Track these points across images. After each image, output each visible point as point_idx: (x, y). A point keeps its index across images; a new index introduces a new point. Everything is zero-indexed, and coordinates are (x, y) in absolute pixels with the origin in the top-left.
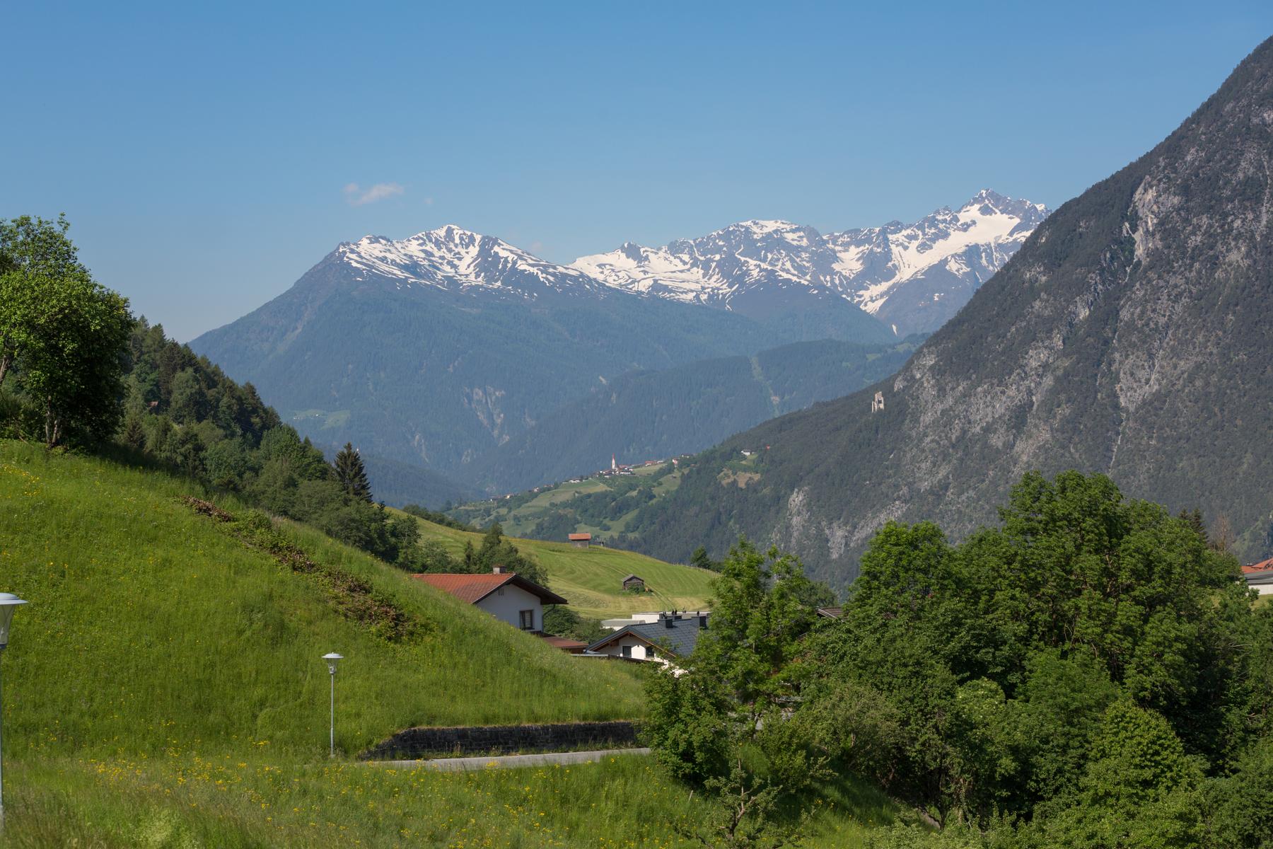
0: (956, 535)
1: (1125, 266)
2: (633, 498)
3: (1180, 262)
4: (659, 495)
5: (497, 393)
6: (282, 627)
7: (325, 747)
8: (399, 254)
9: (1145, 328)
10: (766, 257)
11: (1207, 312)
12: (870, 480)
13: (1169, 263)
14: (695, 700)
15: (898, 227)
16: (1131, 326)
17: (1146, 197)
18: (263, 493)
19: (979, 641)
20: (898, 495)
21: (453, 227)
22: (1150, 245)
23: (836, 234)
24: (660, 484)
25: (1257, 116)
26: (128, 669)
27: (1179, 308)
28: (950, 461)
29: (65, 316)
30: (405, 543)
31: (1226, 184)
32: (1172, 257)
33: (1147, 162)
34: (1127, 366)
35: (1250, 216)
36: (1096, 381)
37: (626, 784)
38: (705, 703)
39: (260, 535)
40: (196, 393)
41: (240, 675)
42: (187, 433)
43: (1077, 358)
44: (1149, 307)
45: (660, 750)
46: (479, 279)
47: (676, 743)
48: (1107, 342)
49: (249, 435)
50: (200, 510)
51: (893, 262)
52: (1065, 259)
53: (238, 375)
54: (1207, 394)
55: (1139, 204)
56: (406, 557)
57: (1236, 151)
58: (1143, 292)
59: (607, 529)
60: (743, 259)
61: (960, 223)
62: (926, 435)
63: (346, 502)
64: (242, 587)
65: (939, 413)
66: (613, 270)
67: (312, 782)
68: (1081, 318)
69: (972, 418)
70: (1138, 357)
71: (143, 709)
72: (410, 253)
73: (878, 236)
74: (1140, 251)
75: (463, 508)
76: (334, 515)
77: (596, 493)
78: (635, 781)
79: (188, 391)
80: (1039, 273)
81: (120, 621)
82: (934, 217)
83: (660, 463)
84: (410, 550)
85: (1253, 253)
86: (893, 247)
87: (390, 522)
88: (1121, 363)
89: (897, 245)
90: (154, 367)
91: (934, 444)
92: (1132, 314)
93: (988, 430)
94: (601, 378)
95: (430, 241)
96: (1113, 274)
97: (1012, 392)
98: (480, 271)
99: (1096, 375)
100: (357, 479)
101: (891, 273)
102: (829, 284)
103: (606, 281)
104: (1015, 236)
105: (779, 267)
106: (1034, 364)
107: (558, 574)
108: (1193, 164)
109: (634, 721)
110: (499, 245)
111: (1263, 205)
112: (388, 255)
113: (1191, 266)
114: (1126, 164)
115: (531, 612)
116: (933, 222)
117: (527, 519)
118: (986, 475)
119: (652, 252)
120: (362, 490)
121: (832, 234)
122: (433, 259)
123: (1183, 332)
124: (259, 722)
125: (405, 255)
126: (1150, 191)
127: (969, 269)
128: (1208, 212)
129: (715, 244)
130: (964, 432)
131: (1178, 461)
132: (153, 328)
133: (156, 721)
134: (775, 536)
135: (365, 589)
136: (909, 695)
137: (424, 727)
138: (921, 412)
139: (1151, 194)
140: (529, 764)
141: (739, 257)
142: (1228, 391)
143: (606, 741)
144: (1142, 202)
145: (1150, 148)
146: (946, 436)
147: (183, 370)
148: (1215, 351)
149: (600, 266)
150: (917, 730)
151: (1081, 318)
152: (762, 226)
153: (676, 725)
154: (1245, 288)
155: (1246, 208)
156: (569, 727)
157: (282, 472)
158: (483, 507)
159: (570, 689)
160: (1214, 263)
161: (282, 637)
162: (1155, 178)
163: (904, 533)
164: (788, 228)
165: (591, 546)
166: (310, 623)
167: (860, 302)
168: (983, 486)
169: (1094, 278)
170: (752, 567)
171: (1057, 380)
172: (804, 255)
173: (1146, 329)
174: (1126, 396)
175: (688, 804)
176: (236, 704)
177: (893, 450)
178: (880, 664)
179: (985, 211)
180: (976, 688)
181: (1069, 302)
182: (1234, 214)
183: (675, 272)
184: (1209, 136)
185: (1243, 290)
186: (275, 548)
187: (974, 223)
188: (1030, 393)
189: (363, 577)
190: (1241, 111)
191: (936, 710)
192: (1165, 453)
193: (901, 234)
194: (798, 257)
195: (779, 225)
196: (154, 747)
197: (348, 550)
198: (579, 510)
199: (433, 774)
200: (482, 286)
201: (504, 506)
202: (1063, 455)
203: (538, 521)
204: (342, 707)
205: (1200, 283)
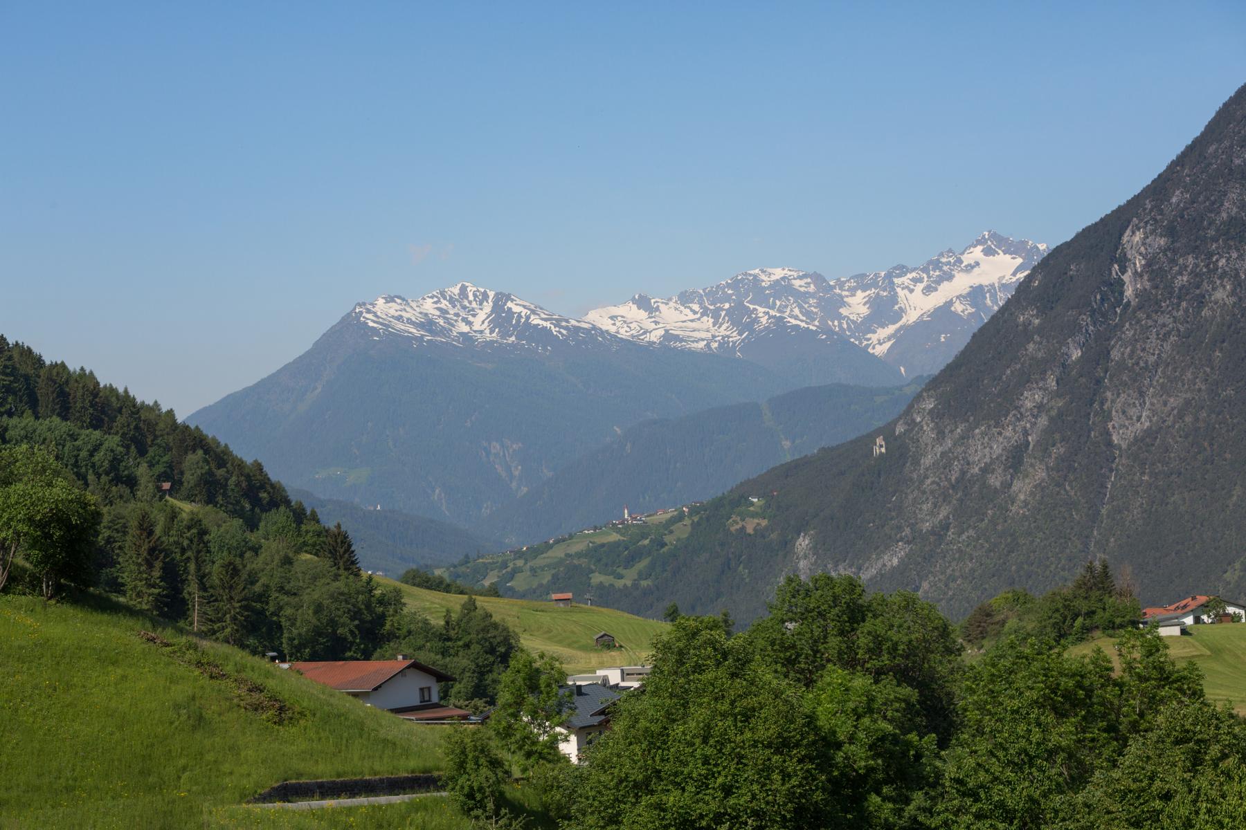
0: (957, 574)
1: (1115, 308)
2: (645, 546)
3: (1168, 302)
5: (514, 446)
6: (200, 718)
8: (414, 312)
9: (1135, 367)
10: (774, 304)
12: (874, 522)
13: (1157, 303)
15: (902, 270)
16: (1121, 365)
17: (1134, 239)
18: (263, 571)
20: (901, 537)
21: (467, 284)
22: (1138, 286)
23: (842, 279)
24: (671, 532)
25: (1238, 157)
27: (1167, 347)
28: (950, 502)
29: (54, 514)
30: (391, 611)
31: (1210, 224)
34: (1118, 405)
35: (1235, 255)
36: (1089, 419)
39: (190, 655)
40: (206, 473)
42: (192, 519)
43: (1070, 398)
44: (1138, 346)
46: (493, 335)
47: (462, 787)
48: (1098, 382)
50: (148, 639)
51: (899, 305)
53: (245, 452)
55: (1127, 246)
57: (1219, 192)
58: (1132, 332)
59: (621, 577)
60: (752, 307)
63: (336, 577)
65: (938, 455)
66: (625, 322)
68: (1073, 358)
69: (971, 459)
70: (1129, 396)
71: (107, 775)
72: (425, 311)
73: (884, 279)
74: (1129, 292)
75: (481, 560)
77: (609, 543)
79: (199, 472)
80: (1032, 316)
82: (938, 260)
83: (671, 512)
84: (397, 618)
85: (1238, 290)
86: (898, 290)
87: (378, 592)
89: (903, 289)
90: (168, 449)
92: (1123, 354)
93: (986, 470)
94: (615, 428)
95: (445, 298)
96: (1104, 315)
97: (1009, 432)
98: (495, 327)
99: (1089, 414)
102: (837, 329)
103: (618, 332)
105: (787, 314)
106: (1029, 404)
108: (1178, 205)
109: (436, 774)
110: (512, 300)
112: (403, 314)
113: (1179, 305)
117: (543, 570)
118: (985, 514)
119: (663, 303)
121: (838, 280)
122: (448, 316)
124: (182, 781)
125: (421, 313)
126: (1138, 233)
127: (973, 310)
128: (1193, 252)
130: (963, 473)
132: (166, 413)
137: (294, 781)
138: (922, 455)
139: (1138, 236)
141: (748, 305)
142: (1217, 426)
143: (429, 787)
145: (1137, 191)
146: (946, 477)
148: (1203, 387)
149: (612, 318)
151: (1073, 358)
153: (464, 776)
155: (1230, 247)
156: (400, 778)
157: (278, 552)
158: (500, 560)
159: (406, 753)
160: (1201, 301)
162: (1142, 220)
166: (220, 714)
167: (868, 346)
168: (983, 525)
169: (1085, 319)
171: (1051, 419)
172: (812, 301)
173: (1137, 369)
174: (1119, 433)
176: (167, 769)
179: (988, 252)
182: (1218, 253)
183: (685, 321)
184: (1193, 178)
185: (1229, 327)
186: (199, 664)
187: (977, 264)
188: (1026, 433)
189: (259, 682)
190: (1223, 152)
193: (906, 277)
194: (805, 303)
199: (287, 811)
200: (496, 342)
201: (520, 557)
202: (1058, 493)
203: (553, 572)
205: (1188, 322)
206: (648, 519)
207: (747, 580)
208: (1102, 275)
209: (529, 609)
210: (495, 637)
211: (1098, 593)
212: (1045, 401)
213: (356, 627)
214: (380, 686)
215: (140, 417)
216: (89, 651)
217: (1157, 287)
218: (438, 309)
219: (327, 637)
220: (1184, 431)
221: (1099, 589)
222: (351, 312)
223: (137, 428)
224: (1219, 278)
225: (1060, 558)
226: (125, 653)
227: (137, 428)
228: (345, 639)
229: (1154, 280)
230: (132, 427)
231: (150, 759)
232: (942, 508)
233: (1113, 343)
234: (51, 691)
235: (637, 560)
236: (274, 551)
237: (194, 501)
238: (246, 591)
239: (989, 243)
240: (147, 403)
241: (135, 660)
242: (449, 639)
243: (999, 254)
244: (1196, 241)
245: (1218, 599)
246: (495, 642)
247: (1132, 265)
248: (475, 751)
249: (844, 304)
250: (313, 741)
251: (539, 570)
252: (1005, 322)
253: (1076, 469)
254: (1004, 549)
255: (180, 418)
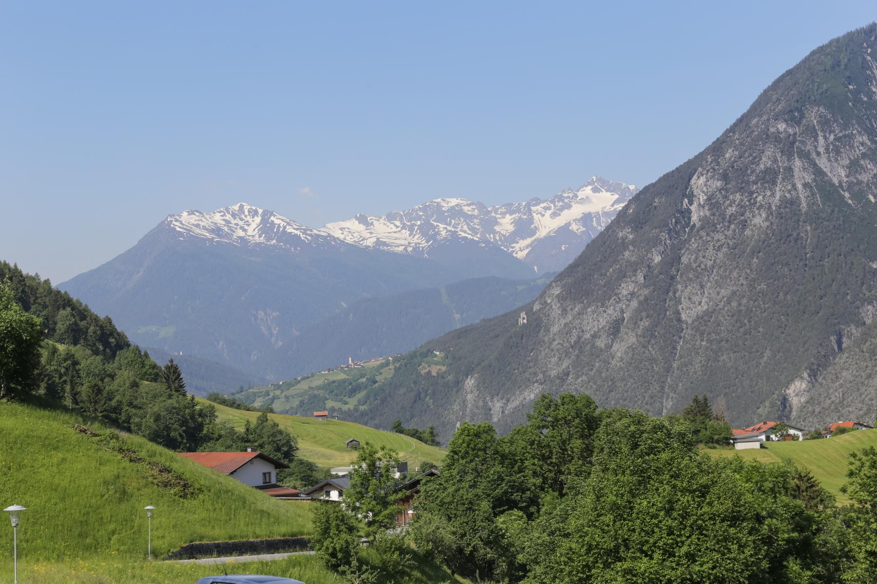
1: (685, 228)
2: (363, 383)
4: (380, 380)
5: (274, 314)
6: (124, 492)
7: (146, 554)
8: (208, 222)
9: (698, 268)
10: (451, 222)
11: (739, 257)
13: (714, 225)
14: (338, 526)
15: (538, 202)
16: (689, 267)
17: (699, 183)
18: (117, 391)
19: (513, 489)
21: (244, 204)
22: (701, 214)
24: (381, 374)
25: (773, 127)
26: (45, 517)
27: (720, 255)
28: (570, 357)
29: (8, 331)
30: (208, 421)
31: (752, 172)
32: (716, 221)
33: (700, 158)
34: (686, 294)
35: (768, 193)
36: (666, 303)
37: (300, 570)
38: (343, 527)
39: (113, 443)
40: (73, 324)
41: (102, 518)
42: (68, 354)
43: (653, 289)
44: (700, 254)
45: (319, 552)
48: (673, 278)
49: (108, 350)
50: (81, 431)
51: (534, 225)
52: (645, 223)
53: (99, 309)
54: (740, 311)
55: (694, 187)
56: (208, 430)
58: (696, 245)
59: (346, 403)
60: (435, 224)
61: (578, 199)
62: (554, 340)
63: (170, 397)
64: (103, 472)
65: (562, 325)
66: (350, 232)
67: (138, 572)
68: (656, 262)
69: (584, 328)
70: (693, 287)
71: (52, 537)
72: (215, 222)
73: (525, 207)
74: (694, 218)
75: (251, 390)
76: (162, 405)
78: (305, 568)
79: (68, 323)
80: (628, 233)
81: (40, 492)
84: (211, 426)
85: (770, 217)
86: (534, 215)
87: (198, 408)
88: (682, 291)
89: (537, 214)
91: (560, 345)
92: (690, 259)
93: (594, 336)
94: (342, 303)
95: (229, 213)
96: (677, 233)
97: (610, 311)
98: (262, 233)
99: (666, 299)
100: (177, 381)
101: (533, 233)
102: (492, 240)
104: (615, 206)
105: (459, 229)
106: (625, 292)
107: (306, 438)
108: (730, 159)
109: (305, 537)
110: (274, 216)
111: (777, 186)
112: (201, 223)
113: (729, 227)
114: (686, 160)
115: (270, 473)
116: (561, 198)
117: (293, 398)
119: (375, 220)
120: (180, 389)
122: (231, 225)
123: (724, 271)
124: (112, 542)
125: (212, 223)
126: (702, 178)
127: (584, 229)
128: (740, 191)
129: (417, 214)
130: (579, 338)
131: (720, 355)
133: (59, 543)
134: (456, 407)
135: (168, 471)
136: (466, 520)
137: (198, 542)
138: (551, 325)
139: (702, 180)
140: (250, 560)
141: (433, 222)
142: (754, 309)
143: (295, 547)
144: (696, 185)
146: (568, 340)
147: (64, 309)
148: (745, 283)
149: (341, 229)
150: (470, 539)
151: (656, 262)
152: (448, 202)
154: (765, 240)
155: (765, 188)
157: (129, 378)
158: (264, 390)
159: (277, 521)
160: (744, 225)
161: (124, 498)
163: (473, 429)
164: (465, 203)
165: (328, 419)
166: (139, 490)
167: (513, 252)
168: (592, 373)
169: (664, 236)
170: (371, 456)
171: (640, 303)
172: (475, 221)
175: (334, 579)
176: (100, 533)
177: (533, 350)
178: (450, 503)
179: (595, 190)
180: (511, 515)
181: (648, 251)
182: (757, 192)
185: (764, 242)
186: (121, 450)
188: (622, 311)
189: (167, 464)
190: (762, 123)
191: (480, 528)
192: (712, 350)
193: (540, 206)
195: (459, 201)
196: (58, 556)
197: (160, 449)
198: (328, 391)
199: (199, 566)
200: (263, 243)
201: (278, 389)
202: (644, 352)
203: (301, 399)
204: (155, 533)
205: (735, 238)
206: (365, 364)
207: (432, 407)
208: (676, 206)
209: (298, 422)
210: (280, 440)
211: (702, 418)
212: (636, 290)
213: (184, 431)
214: (235, 471)
215: (25, 284)
216: (35, 439)
217: (714, 215)
218: (223, 220)
219: (163, 438)
220: (731, 312)
221: (702, 415)
222: (165, 220)
223: (23, 291)
224: (757, 209)
225: (644, 396)
226: (64, 441)
227: (23, 291)
228: (176, 440)
229: (712, 209)
230: (20, 291)
231: (87, 525)
232: (565, 361)
233: (683, 252)
234: (6, 469)
235: (358, 392)
236: (126, 378)
237: (64, 343)
238: (107, 404)
239: (596, 184)
240: (30, 274)
241: (72, 446)
242: (248, 441)
243: (602, 192)
244: (742, 184)
245: (783, 424)
246: (280, 443)
247: (697, 200)
248: (336, 520)
249: (497, 223)
250: (210, 511)
251: (290, 398)
252: (609, 236)
253: (656, 337)
254: (606, 389)
255: (54, 284)
